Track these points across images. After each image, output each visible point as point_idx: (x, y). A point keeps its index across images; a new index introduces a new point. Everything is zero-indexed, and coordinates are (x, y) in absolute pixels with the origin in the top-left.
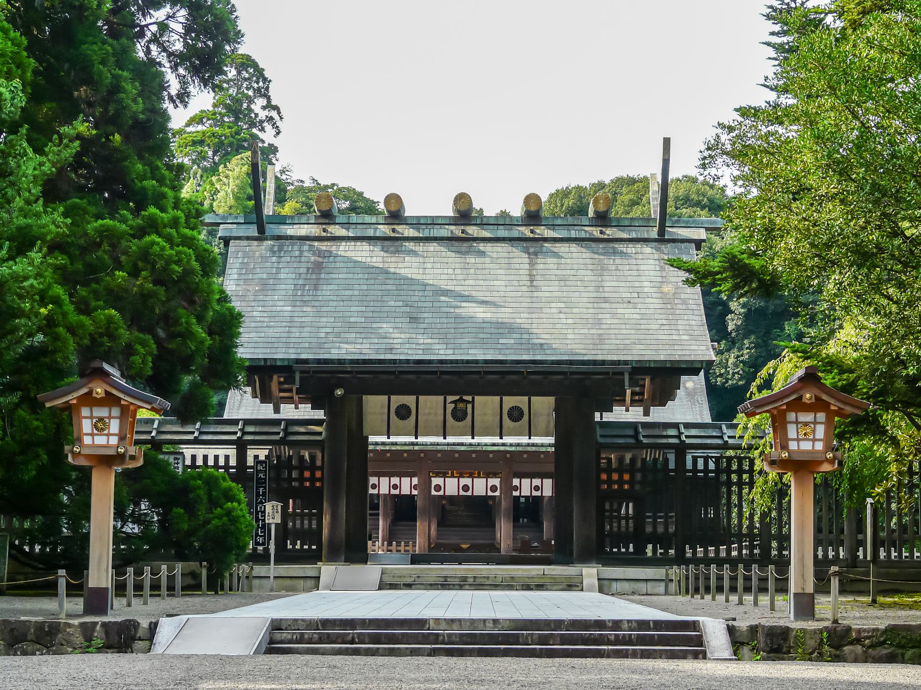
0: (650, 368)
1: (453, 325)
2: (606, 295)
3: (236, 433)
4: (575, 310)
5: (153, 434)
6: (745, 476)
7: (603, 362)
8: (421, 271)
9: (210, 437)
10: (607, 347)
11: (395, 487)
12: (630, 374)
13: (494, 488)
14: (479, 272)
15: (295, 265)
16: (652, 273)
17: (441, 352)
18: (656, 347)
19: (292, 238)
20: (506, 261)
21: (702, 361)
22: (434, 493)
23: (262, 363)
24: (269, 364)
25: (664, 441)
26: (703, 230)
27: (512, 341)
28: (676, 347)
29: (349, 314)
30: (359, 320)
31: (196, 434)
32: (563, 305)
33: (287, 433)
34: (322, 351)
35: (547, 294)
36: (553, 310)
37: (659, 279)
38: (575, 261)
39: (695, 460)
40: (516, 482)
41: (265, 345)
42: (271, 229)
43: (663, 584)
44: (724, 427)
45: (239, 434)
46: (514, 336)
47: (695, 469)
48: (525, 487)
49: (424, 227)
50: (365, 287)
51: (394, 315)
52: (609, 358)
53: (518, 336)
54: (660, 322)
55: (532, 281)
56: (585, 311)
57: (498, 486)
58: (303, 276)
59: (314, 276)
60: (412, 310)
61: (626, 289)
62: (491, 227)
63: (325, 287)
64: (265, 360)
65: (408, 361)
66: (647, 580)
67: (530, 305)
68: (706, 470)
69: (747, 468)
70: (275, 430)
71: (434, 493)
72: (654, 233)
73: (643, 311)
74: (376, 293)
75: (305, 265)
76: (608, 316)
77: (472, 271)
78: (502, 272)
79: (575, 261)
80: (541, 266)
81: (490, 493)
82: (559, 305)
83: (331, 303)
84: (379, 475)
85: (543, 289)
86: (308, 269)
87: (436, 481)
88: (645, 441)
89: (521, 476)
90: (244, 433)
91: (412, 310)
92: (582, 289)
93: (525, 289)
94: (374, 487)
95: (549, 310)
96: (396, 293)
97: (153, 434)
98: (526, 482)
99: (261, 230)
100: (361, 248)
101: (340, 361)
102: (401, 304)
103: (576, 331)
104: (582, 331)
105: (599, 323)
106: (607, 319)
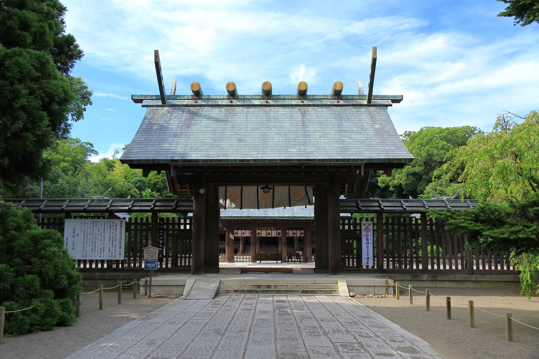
0: (375, 164)
2: (344, 129)
3: (150, 206)
4: (329, 136)
7: (349, 160)
8: (245, 119)
9: (137, 208)
10: (349, 152)
11: (294, 234)
12: (365, 167)
13: (279, 234)
16: (366, 119)
17: (255, 156)
18: (378, 152)
19: (179, 106)
20: (290, 115)
21: (406, 159)
22: (257, 235)
23: (152, 162)
24: (155, 163)
25: (372, 208)
26: (390, 101)
27: (295, 150)
28: (389, 152)
30: (210, 141)
32: (321, 134)
33: (177, 206)
35: (312, 129)
37: (371, 122)
38: (325, 115)
39: (387, 218)
40: (287, 231)
41: (155, 153)
43: (384, 289)
44: (402, 202)
45: (152, 207)
46: (296, 148)
48: (291, 233)
52: (352, 158)
53: (298, 148)
54: (377, 141)
55: (304, 123)
56: (334, 136)
58: (183, 122)
59: (189, 122)
60: (239, 136)
63: (193, 127)
64: (153, 160)
65: (236, 160)
67: (304, 134)
70: (171, 204)
71: (257, 235)
72: (365, 102)
73: (366, 136)
75: (184, 117)
76: (347, 138)
78: (288, 119)
79: (325, 115)
80: (308, 117)
81: (278, 236)
82: (319, 134)
83: (196, 134)
84: (238, 229)
86: (186, 119)
87: (258, 231)
88: (363, 209)
89: (289, 229)
90: (155, 206)
91: (239, 136)
92: (331, 127)
93: (300, 127)
94: (302, 233)
96: (231, 129)
99: (164, 102)
101: (196, 160)
102: (233, 134)
103: (331, 145)
104: (334, 145)
105: (343, 141)
106: (347, 139)
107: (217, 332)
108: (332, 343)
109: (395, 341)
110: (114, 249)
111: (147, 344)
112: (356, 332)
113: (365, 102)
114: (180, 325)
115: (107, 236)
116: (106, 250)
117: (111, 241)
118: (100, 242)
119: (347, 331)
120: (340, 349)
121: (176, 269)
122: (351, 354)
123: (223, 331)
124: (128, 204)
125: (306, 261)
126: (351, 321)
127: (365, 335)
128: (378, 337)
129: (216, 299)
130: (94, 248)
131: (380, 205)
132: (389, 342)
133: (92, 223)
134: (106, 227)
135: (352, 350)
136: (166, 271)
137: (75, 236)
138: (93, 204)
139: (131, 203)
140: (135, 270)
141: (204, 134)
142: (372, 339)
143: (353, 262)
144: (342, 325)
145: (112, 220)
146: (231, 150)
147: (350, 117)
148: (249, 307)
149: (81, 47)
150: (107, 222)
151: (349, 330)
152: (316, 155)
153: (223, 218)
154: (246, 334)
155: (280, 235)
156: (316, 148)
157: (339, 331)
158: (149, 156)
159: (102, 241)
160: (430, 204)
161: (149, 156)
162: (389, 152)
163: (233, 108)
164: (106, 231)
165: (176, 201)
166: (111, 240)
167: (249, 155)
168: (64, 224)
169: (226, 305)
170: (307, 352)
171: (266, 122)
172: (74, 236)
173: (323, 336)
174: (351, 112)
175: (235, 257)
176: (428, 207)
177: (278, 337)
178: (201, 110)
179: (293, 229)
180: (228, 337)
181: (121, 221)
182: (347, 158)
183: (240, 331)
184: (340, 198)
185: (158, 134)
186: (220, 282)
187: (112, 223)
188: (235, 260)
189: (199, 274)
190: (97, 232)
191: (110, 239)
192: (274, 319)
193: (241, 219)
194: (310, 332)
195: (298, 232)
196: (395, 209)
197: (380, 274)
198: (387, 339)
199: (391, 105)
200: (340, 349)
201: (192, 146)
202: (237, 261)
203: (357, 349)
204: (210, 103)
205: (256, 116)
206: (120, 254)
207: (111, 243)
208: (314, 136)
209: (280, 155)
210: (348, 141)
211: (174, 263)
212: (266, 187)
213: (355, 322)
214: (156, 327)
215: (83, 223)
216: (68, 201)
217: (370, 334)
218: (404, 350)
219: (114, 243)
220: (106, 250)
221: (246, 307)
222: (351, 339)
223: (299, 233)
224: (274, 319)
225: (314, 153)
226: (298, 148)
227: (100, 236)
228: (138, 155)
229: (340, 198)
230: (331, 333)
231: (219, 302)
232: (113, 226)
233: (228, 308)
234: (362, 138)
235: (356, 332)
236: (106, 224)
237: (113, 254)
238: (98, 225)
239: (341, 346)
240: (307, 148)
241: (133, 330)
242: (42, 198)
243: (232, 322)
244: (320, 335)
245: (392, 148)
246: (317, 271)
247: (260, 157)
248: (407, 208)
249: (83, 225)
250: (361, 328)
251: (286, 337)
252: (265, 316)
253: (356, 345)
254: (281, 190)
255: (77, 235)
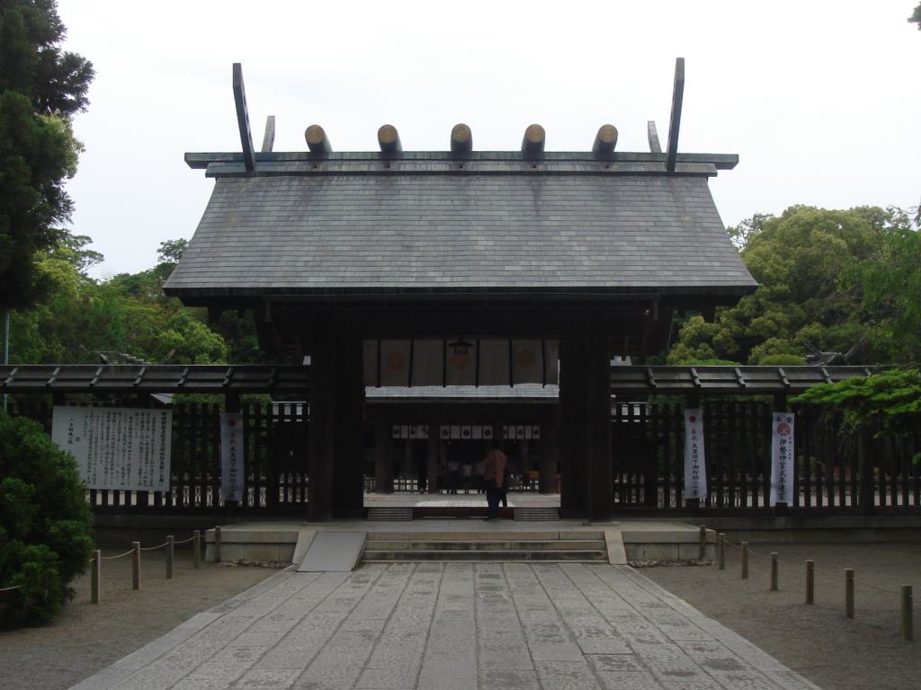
1: (451, 253)
5: (137, 382)
6: (660, 422)
11: (520, 432)
13: (487, 433)
14: (479, 203)
15: (283, 198)
17: (437, 279)
22: (442, 437)
25: (678, 385)
28: (710, 273)
29: (334, 243)
31: (181, 382)
34: (298, 279)
35: (555, 224)
36: (563, 238)
40: (505, 428)
42: (260, 168)
46: (522, 263)
47: (282, 415)
48: (512, 433)
49: (420, 162)
50: (353, 218)
51: (385, 243)
55: (537, 211)
57: (491, 431)
61: (642, 219)
62: (492, 162)
66: (678, 544)
68: (282, 415)
69: (626, 414)
72: (663, 169)
74: (366, 223)
76: (625, 243)
77: (473, 202)
80: (548, 198)
85: (551, 218)
88: (658, 386)
89: (509, 424)
95: (558, 238)
97: (137, 382)
98: (512, 428)
100: (354, 183)
107: (366, 635)
108: (583, 654)
109: (701, 649)
110: (149, 469)
111: (236, 655)
112: (631, 634)
113: (663, 169)
114: (293, 623)
115: (136, 442)
116: (134, 469)
117: (144, 453)
118: (121, 453)
119: (615, 632)
120: (599, 664)
121: (275, 512)
122: (615, 675)
123: (377, 634)
124: (177, 376)
125: (543, 490)
126: (625, 613)
127: (647, 639)
128: (673, 642)
129: (359, 572)
130: (109, 466)
131: (694, 378)
132: (691, 652)
133: (106, 416)
134: (134, 424)
135: (619, 667)
136: (255, 515)
137: (74, 440)
138: (106, 376)
139: (184, 374)
140: (191, 510)
141: (331, 233)
142: (659, 646)
143: (638, 496)
144: (607, 621)
145: (146, 411)
146: (389, 269)
147: (631, 199)
148: (427, 588)
149: (64, 21)
150: (137, 414)
151: (619, 629)
152: (562, 279)
153: (370, 401)
154: (421, 641)
155: (490, 437)
156: (562, 263)
157: (599, 632)
158: (222, 280)
159: (127, 453)
160: (793, 377)
161: (222, 280)
162: (710, 273)
163: (392, 178)
164: (134, 432)
165: (274, 370)
166: (144, 451)
167: (424, 279)
168: (51, 416)
169: (380, 582)
170: (537, 672)
171: (460, 208)
172: (70, 442)
173: (567, 643)
174: (633, 188)
175: (396, 481)
176: (790, 381)
177: (482, 644)
178: (325, 183)
179: (516, 424)
180: (387, 645)
181: (164, 414)
182: (626, 284)
183: (409, 635)
184: (613, 363)
185: (238, 234)
186: (368, 536)
187: (145, 417)
188: (396, 487)
189: (322, 521)
190: (116, 434)
191: (141, 448)
192: (476, 611)
193: (408, 402)
194: (544, 636)
195: (528, 428)
196: (724, 385)
197: (692, 519)
198: (689, 647)
199: (715, 175)
200: (599, 664)
201: (306, 259)
202: (399, 490)
203: (629, 665)
204: (344, 169)
205: (438, 196)
206: (162, 480)
207: (144, 457)
208: (558, 238)
209: (489, 278)
210: (627, 248)
211: (272, 496)
212: (460, 343)
213: (632, 616)
214: (247, 624)
215: (89, 414)
216: (57, 370)
217: (659, 637)
218: (716, 665)
219: (150, 457)
220: (134, 469)
221: (421, 587)
222: (621, 647)
223: (529, 433)
224: (476, 611)
225: (559, 273)
226: (527, 263)
227: (121, 442)
228: (200, 280)
229: (613, 363)
230: (584, 635)
231: (367, 578)
232: (148, 422)
233: (384, 589)
234: (655, 243)
235: (631, 634)
236: (134, 417)
237: (149, 480)
238: (117, 420)
239: (600, 659)
240: (545, 263)
241: (206, 630)
242: (6, 364)
243: (394, 618)
244: (561, 641)
245: (715, 264)
246: (565, 513)
247: (447, 282)
248: (748, 385)
249: (89, 420)
250: (642, 627)
251: (498, 644)
252: (456, 606)
253: (629, 658)
254: (494, 349)
255: (78, 439)
